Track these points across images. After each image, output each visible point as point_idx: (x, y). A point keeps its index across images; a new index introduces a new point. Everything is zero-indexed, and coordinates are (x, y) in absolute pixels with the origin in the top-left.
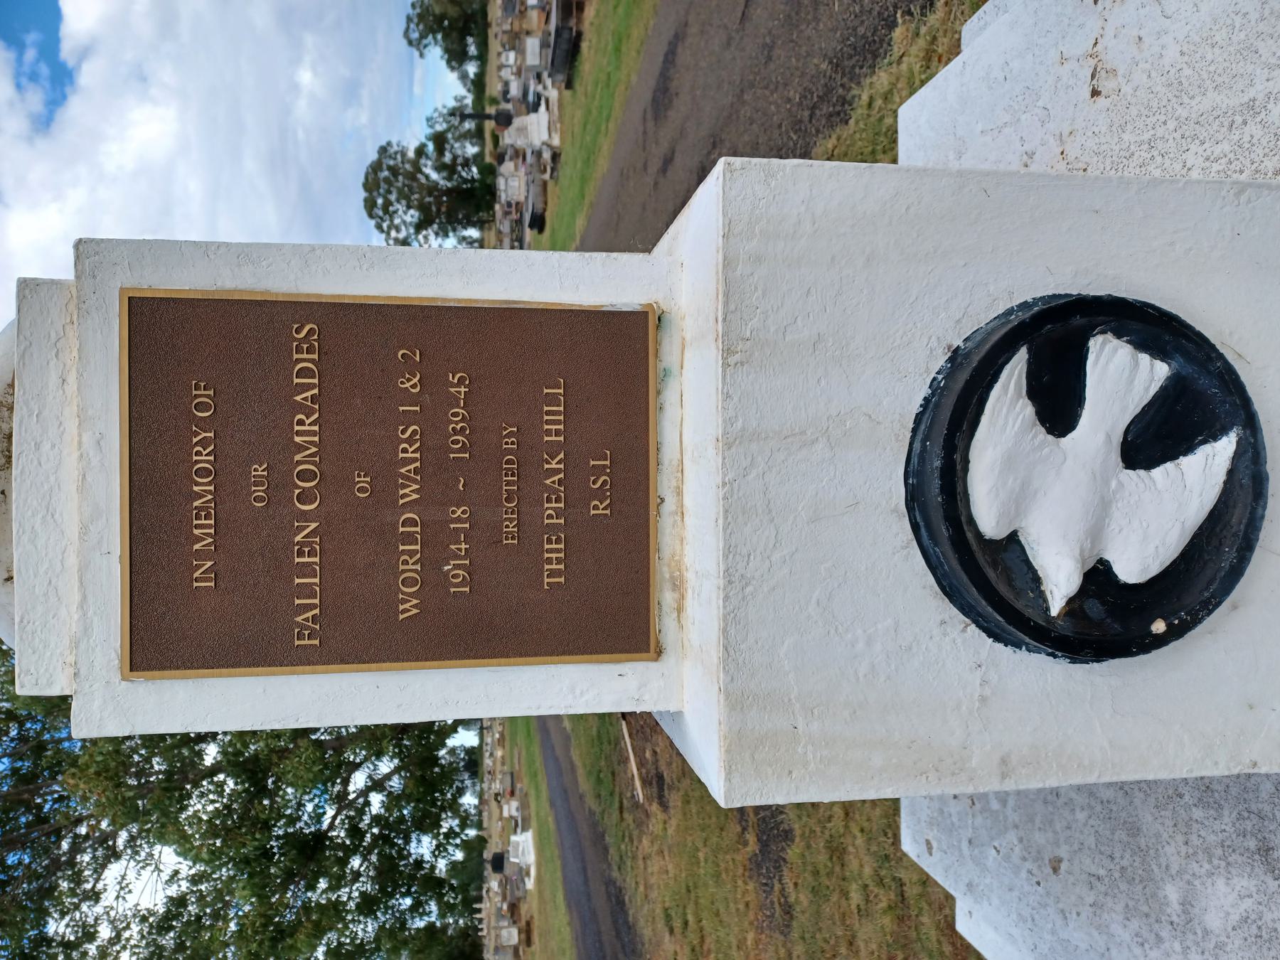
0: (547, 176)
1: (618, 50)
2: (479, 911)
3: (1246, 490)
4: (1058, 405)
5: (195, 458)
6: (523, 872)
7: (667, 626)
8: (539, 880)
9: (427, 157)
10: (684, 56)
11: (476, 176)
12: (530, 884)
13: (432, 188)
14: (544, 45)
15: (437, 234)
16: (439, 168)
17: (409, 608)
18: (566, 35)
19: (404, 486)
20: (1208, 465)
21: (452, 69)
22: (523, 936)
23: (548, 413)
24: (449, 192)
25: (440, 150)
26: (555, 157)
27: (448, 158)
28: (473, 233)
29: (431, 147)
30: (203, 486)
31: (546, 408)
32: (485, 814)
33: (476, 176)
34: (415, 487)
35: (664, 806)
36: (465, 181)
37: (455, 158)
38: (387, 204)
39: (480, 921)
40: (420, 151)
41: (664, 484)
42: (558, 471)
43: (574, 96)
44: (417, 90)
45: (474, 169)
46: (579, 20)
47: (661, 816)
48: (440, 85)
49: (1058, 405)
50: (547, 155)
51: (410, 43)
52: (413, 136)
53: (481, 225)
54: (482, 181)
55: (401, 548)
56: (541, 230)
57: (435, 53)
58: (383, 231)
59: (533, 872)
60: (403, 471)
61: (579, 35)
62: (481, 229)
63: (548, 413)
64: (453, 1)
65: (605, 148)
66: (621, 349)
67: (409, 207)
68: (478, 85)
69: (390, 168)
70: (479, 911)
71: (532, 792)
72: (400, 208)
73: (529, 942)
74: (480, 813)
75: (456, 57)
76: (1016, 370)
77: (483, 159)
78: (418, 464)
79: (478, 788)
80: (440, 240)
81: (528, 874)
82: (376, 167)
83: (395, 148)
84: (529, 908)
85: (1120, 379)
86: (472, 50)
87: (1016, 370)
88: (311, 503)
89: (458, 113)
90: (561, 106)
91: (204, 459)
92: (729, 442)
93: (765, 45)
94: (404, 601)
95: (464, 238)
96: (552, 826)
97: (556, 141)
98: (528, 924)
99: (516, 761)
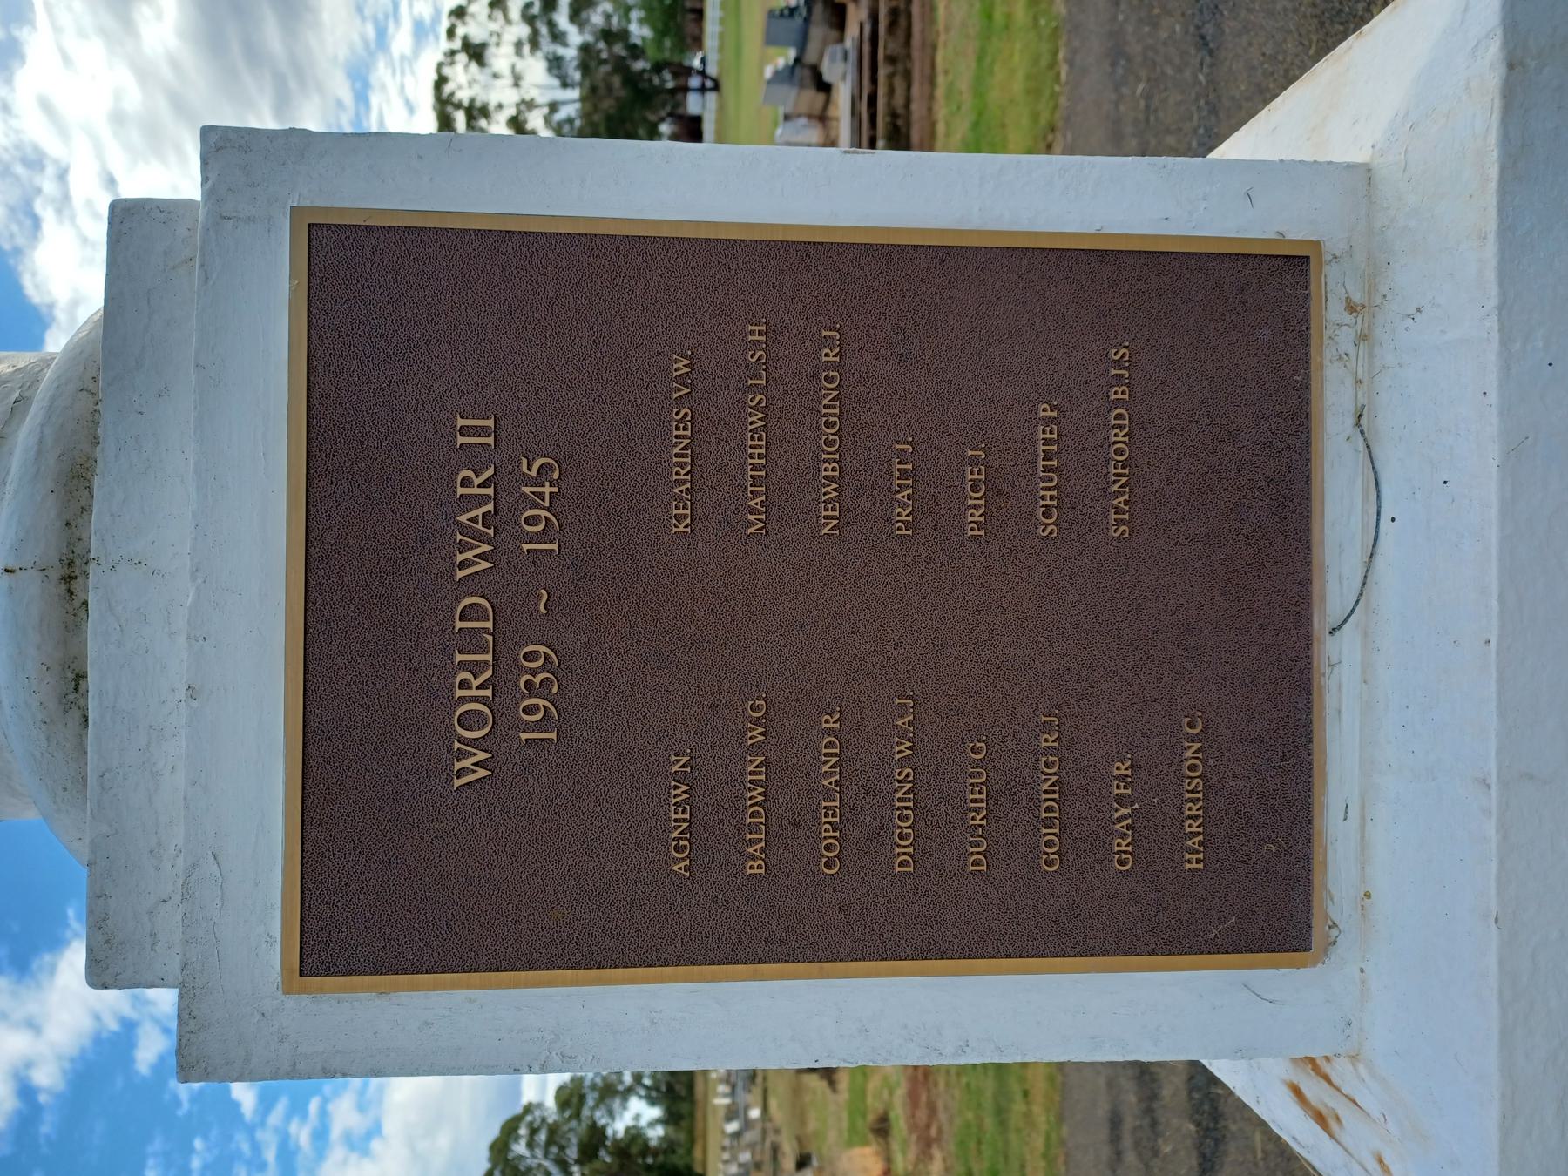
5: (459, 693)
19: (464, 547)
23: (464, 431)
31: (461, 422)
34: (485, 548)
42: (481, 500)
55: (459, 658)
60: (463, 518)
63: (464, 431)
66: (1248, 318)
78: (490, 507)
88: (536, 660)
93: (788, 76)
94: (461, 755)
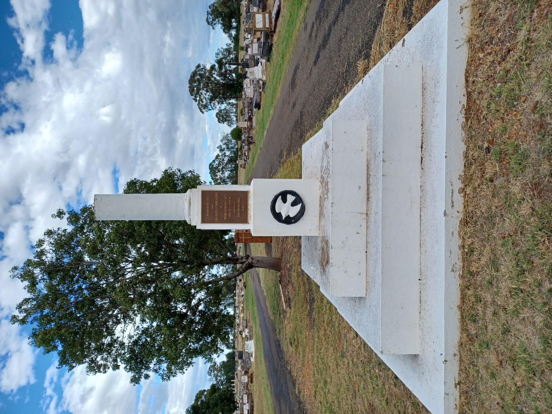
0: (261, 90)
1: (283, 58)
2: (233, 383)
3: (303, 209)
4: (284, 201)
6: (250, 355)
7: (249, 221)
8: (256, 357)
9: (215, 70)
10: (298, 74)
11: (235, 78)
12: (252, 360)
13: (218, 83)
14: (259, 47)
15: (218, 103)
16: (220, 75)
17: (225, 218)
18: (267, 44)
20: (299, 207)
21: (226, 33)
22: (249, 379)
24: (224, 84)
25: (220, 68)
26: (264, 84)
27: (223, 70)
28: (233, 101)
29: (217, 66)
30: (208, 207)
32: (236, 342)
33: (235, 78)
35: (290, 308)
36: (230, 80)
37: (226, 71)
38: (199, 90)
39: (234, 387)
40: (213, 67)
41: (249, 207)
43: (270, 64)
44: (211, 41)
45: (234, 75)
46: (272, 40)
47: (289, 311)
48: (221, 39)
49: (284, 201)
50: (261, 82)
51: (208, 23)
52: (209, 61)
53: (237, 98)
54: (237, 81)
56: (259, 109)
57: (219, 27)
58: (196, 101)
59: (254, 355)
61: (272, 45)
62: (237, 100)
64: (226, 13)
65: (279, 89)
66: (245, 194)
67: (207, 91)
68: (236, 40)
69: (200, 75)
70: (233, 383)
71: (254, 326)
72: (204, 92)
73: (252, 382)
74: (234, 343)
75: (227, 28)
76: (280, 197)
77: (238, 71)
79: (233, 332)
80: (220, 105)
81: (252, 356)
82: (194, 74)
83: (202, 67)
84: (253, 369)
85: (290, 198)
86: (234, 24)
87: (280, 197)
89: (228, 51)
90: (266, 65)
91: (208, 205)
92: (254, 204)
95: (230, 103)
96: (260, 334)
97: (264, 79)
98: (252, 375)
99: (248, 316)
